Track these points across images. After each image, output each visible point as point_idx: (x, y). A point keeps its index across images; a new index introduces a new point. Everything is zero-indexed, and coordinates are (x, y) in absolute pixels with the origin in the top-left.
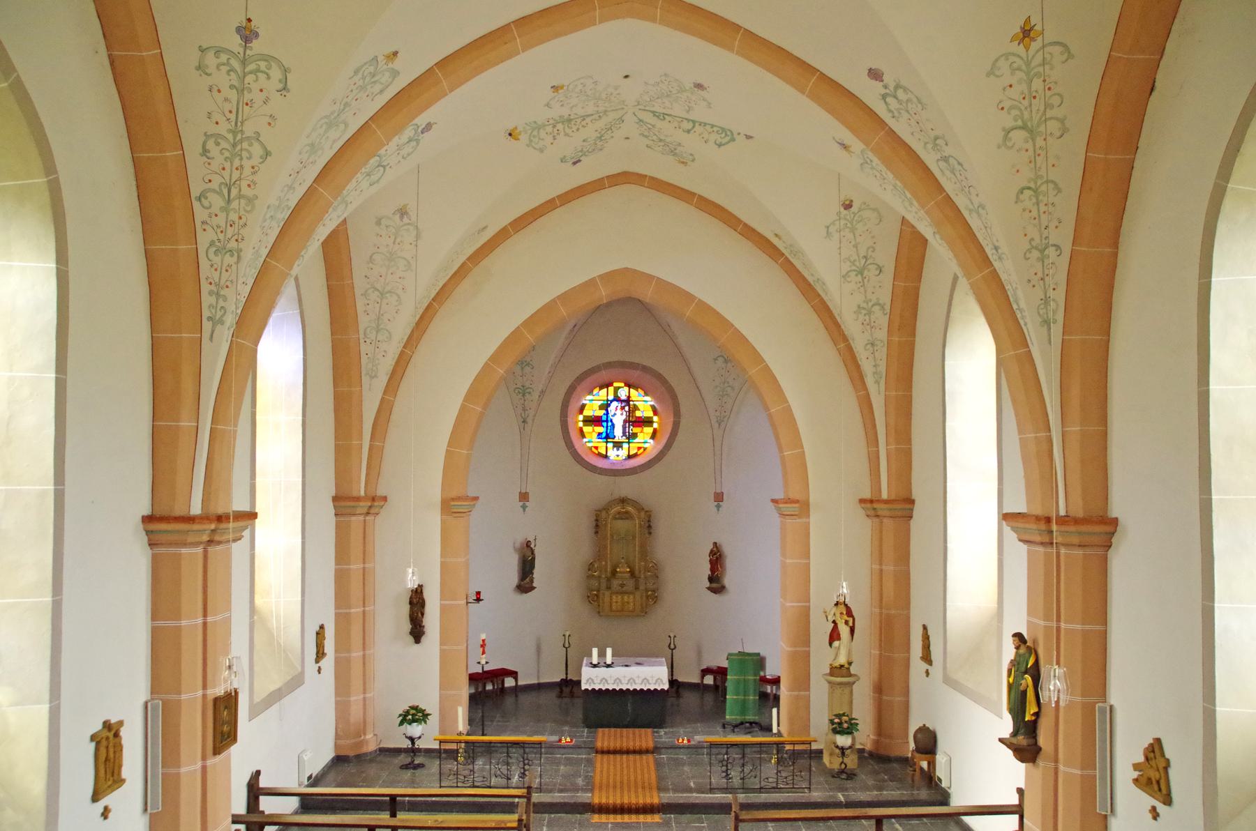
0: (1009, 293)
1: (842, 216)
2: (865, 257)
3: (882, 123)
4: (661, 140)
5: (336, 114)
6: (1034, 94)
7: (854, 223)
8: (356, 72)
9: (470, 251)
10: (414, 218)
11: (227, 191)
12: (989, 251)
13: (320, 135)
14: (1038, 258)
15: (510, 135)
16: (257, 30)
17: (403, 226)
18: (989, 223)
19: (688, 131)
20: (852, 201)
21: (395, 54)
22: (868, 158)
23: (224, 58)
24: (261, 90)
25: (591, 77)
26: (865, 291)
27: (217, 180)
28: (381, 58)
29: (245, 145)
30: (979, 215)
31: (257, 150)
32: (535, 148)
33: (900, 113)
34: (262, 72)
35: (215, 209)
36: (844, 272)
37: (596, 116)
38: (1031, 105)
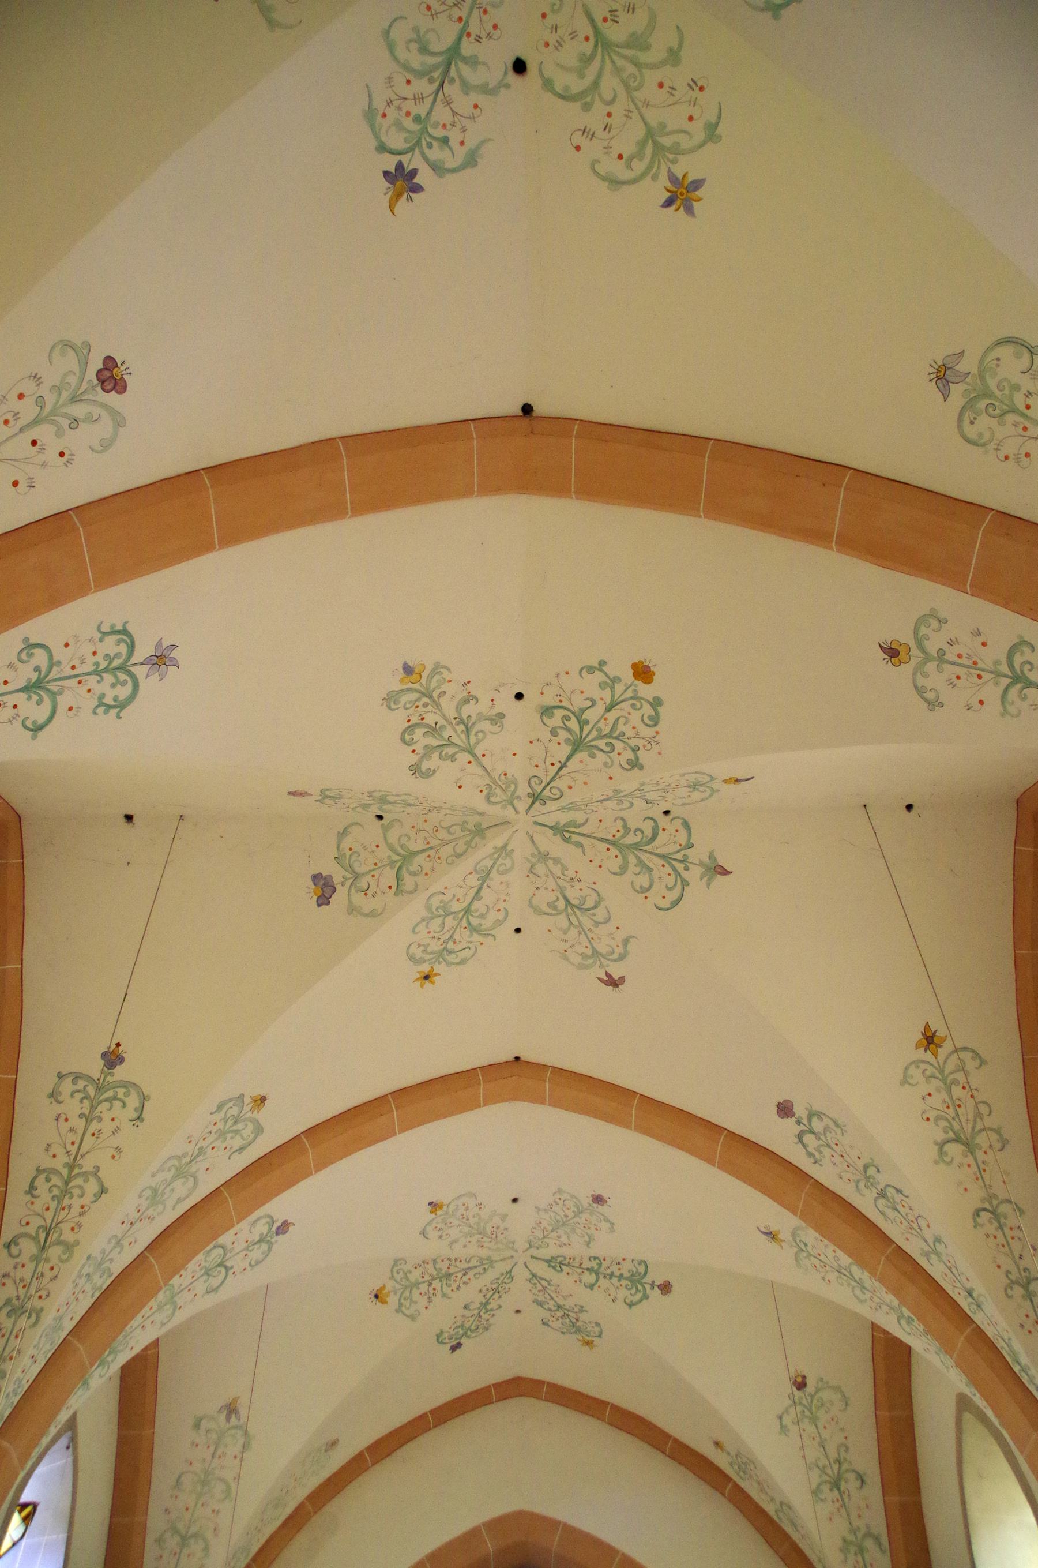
0: (1004, 1352)
1: (796, 1398)
2: (838, 1461)
3: (805, 1176)
4: (559, 1307)
5: (188, 1159)
6: (958, 1102)
7: (814, 1409)
8: (220, 1107)
9: (313, 1482)
10: (243, 1420)
11: (44, 1237)
12: (964, 1302)
13: (166, 1180)
14: (1023, 1296)
15: (376, 1296)
16: (124, 1055)
17: (229, 1429)
18: (952, 1260)
19: (591, 1287)
20: (804, 1377)
21: (263, 1099)
22: (800, 1241)
23: (81, 1084)
24: (113, 1120)
25: (474, 1196)
26: (849, 1515)
27: (36, 1222)
28: (247, 1100)
29: (79, 1181)
30: (938, 1254)
31: (92, 1187)
32: (405, 1315)
33: (820, 1152)
34: (118, 1099)
35: (24, 1258)
36: (814, 1486)
37: (480, 1270)
38: (958, 1115)
